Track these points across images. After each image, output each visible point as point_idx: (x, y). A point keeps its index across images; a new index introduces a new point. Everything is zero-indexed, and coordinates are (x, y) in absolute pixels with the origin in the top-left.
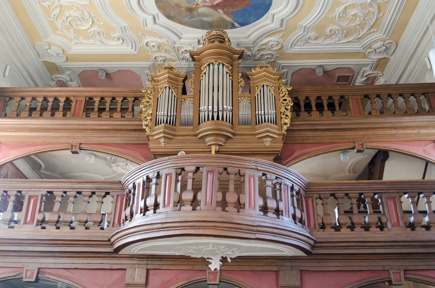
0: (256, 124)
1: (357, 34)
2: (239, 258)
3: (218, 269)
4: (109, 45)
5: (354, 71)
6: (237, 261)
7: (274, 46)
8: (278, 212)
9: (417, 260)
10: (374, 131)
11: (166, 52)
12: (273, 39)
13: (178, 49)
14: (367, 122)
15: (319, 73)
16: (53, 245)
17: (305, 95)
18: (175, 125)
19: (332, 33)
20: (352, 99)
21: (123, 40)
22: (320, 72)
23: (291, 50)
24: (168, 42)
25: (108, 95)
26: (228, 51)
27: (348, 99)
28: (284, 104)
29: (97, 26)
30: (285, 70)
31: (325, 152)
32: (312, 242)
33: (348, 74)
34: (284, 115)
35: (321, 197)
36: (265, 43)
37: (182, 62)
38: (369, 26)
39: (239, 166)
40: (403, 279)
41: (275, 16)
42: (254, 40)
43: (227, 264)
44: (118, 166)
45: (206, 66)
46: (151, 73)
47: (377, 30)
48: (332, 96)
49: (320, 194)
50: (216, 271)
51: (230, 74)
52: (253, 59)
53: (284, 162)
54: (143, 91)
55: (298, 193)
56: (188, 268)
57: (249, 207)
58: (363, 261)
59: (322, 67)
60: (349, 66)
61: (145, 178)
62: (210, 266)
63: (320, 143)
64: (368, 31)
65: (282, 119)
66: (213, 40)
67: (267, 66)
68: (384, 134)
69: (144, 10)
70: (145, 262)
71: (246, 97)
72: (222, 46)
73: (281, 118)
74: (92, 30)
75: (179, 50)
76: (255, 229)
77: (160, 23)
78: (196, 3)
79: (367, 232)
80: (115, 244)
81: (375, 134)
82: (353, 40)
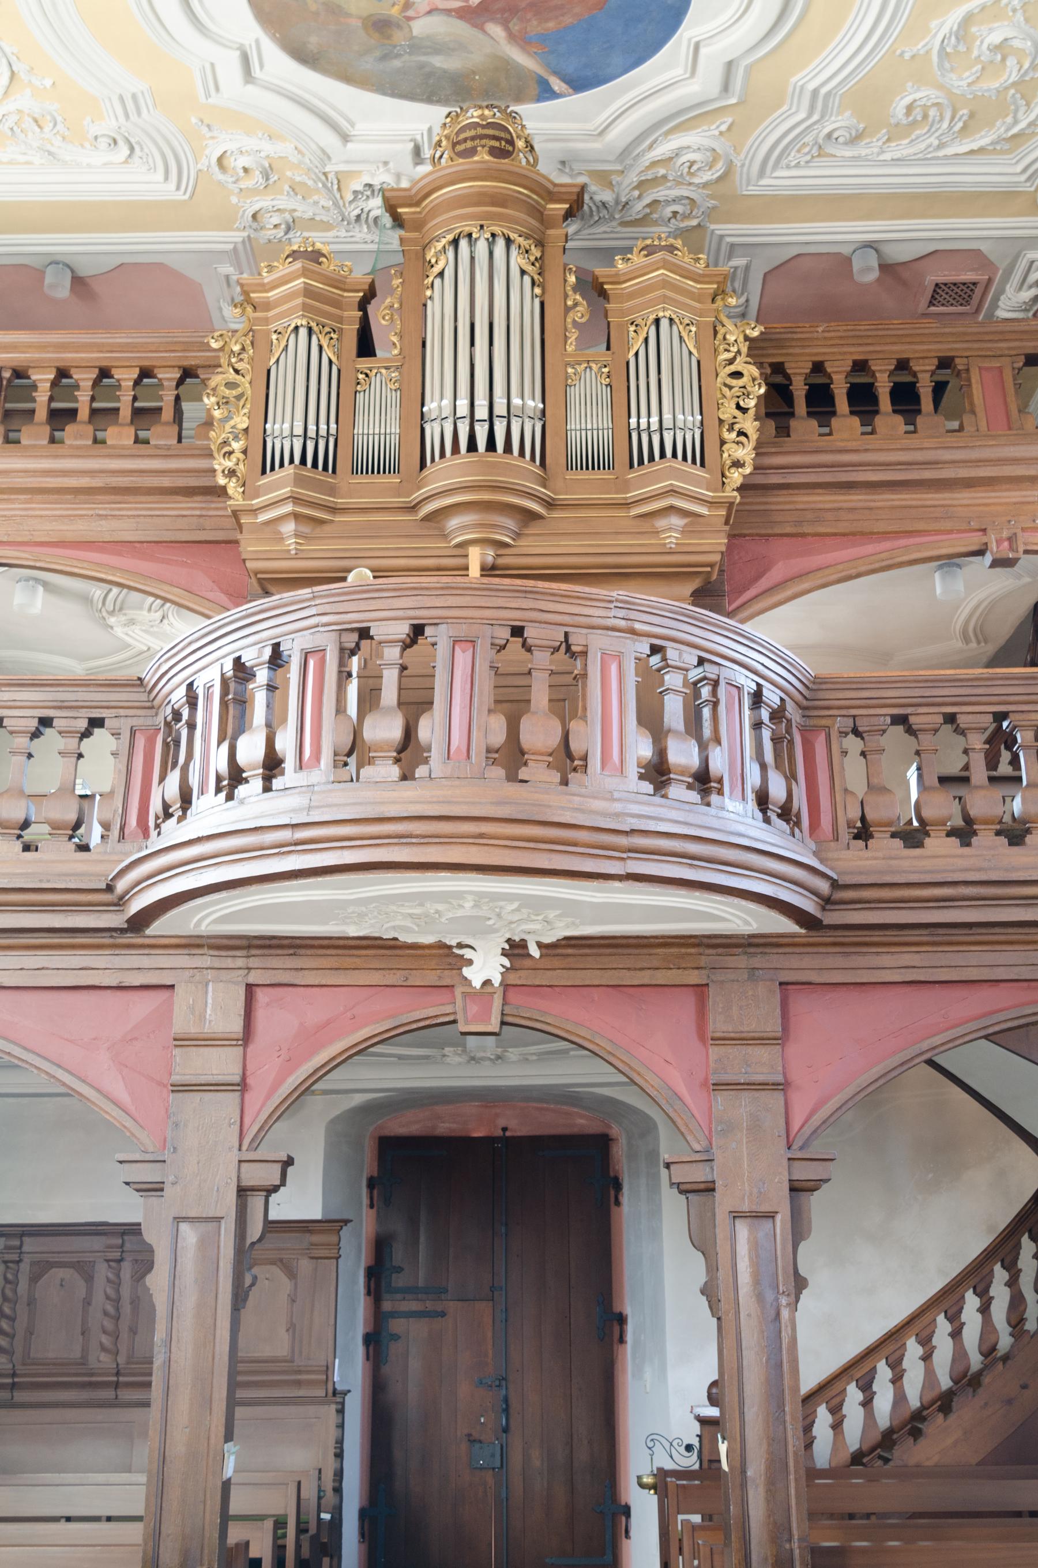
0: (631, 466)
1: (1009, 119)
2: (570, 942)
3: (497, 980)
5: (992, 263)
7: (699, 169)
11: (296, 194)
18: (334, 471)
21: (132, 149)
22: (869, 269)
23: (764, 182)
24: (300, 152)
25: (82, 359)
28: (733, 390)
31: (877, 565)
32: (824, 886)
33: (968, 277)
34: (731, 429)
35: (860, 729)
37: (357, 229)
41: (703, 51)
43: (527, 963)
44: (132, 622)
45: (444, 247)
46: (242, 273)
49: (854, 717)
50: (488, 989)
51: (536, 277)
54: (214, 345)
55: (777, 715)
57: (603, 768)
62: (466, 972)
63: (862, 534)
65: (726, 447)
66: (469, 144)
67: (672, 246)
69: (203, 25)
70: (240, 962)
71: (593, 366)
73: (723, 443)
76: (623, 841)
79: (1015, 849)
82: (992, 143)
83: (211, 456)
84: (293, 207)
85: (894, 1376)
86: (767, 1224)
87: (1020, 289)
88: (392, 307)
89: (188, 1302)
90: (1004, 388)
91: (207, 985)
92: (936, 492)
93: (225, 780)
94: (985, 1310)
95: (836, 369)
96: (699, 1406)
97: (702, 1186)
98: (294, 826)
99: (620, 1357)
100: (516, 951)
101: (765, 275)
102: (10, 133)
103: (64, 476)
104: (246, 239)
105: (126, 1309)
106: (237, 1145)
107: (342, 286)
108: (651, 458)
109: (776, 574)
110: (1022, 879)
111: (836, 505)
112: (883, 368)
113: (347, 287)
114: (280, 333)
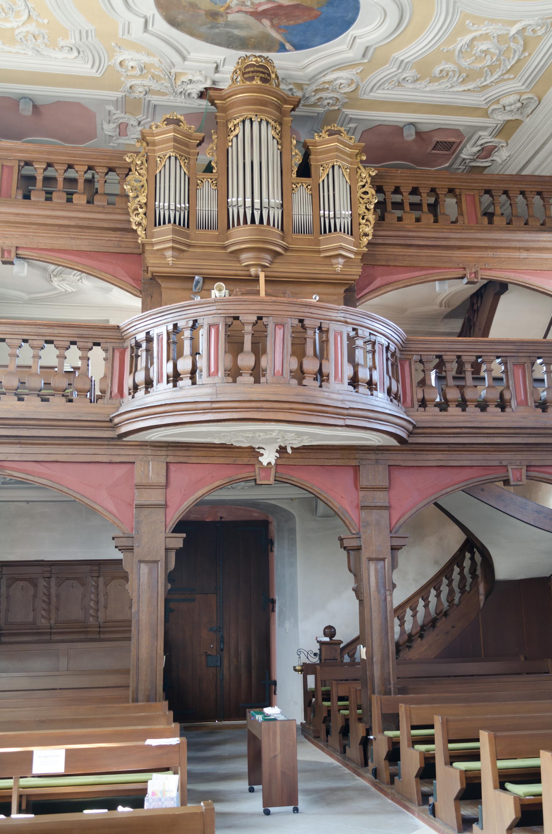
0: (321, 233)
1: (483, 79)
2: (305, 448)
3: (273, 463)
5: (463, 135)
6: (301, 452)
7: (344, 87)
8: (371, 385)
9: (545, 453)
10: (496, 252)
11: (154, 79)
12: (344, 75)
13: (176, 75)
14: (488, 237)
15: (409, 135)
16: (19, 427)
17: (394, 183)
18: (188, 227)
19: (444, 75)
20: (466, 195)
21: (79, 53)
22: (411, 135)
23: (372, 94)
24: (161, 62)
25: (59, 159)
26: (275, 97)
27: (460, 195)
28: (364, 200)
29: (34, 24)
30: (352, 125)
31: (420, 281)
32: (410, 427)
33: (452, 140)
34: (363, 219)
35: (423, 360)
36: (329, 81)
38: (503, 70)
39: (322, 317)
40: (524, 477)
41: (358, 41)
43: (286, 455)
44: (64, 280)
45: (238, 123)
46: (117, 110)
47: (515, 77)
48: (435, 188)
49: (421, 355)
50: (270, 466)
51: (279, 140)
52: (305, 103)
53: (357, 295)
54: (128, 160)
55: (393, 355)
56: (229, 461)
57: (335, 380)
58: (474, 453)
59: (414, 126)
61: (171, 327)
62: (260, 459)
63: (414, 267)
64: (499, 77)
65: (361, 226)
66: (251, 75)
67: (339, 131)
68: (510, 258)
69: (131, 7)
70: (164, 453)
71: (304, 184)
72: (267, 88)
73: (360, 224)
74: (24, 29)
76: (345, 412)
77: (155, 31)
78: (227, 5)
79: (483, 413)
80: (120, 426)
81: (497, 256)
82: (474, 88)
83: (128, 214)
84: (151, 85)
85: (400, 624)
86: (382, 563)
87: (473, 146)
88: (212, 149)
89: (145, 597)
90: (475, 204)
91: (149, 463)
92: (446, 251)
93: (171, 377)
94: (438, 596)
95: (404, 190)
96: (319, 637)
97: (356, 548)
98: (212, 402)
99: (272, 618)
100: (282, 451)
101: (363, 132)
102: (20, 41)
103: (57, 219)
104: (124, 96)
105: (54, 599)
106: (164, 530)
107: (190, 137)
108: (330, 231)
109: (377, 283)
110: (487, 426)
111: (404, 253)
112: (425, 191)
113: (192, 138)
114: (161, 158)
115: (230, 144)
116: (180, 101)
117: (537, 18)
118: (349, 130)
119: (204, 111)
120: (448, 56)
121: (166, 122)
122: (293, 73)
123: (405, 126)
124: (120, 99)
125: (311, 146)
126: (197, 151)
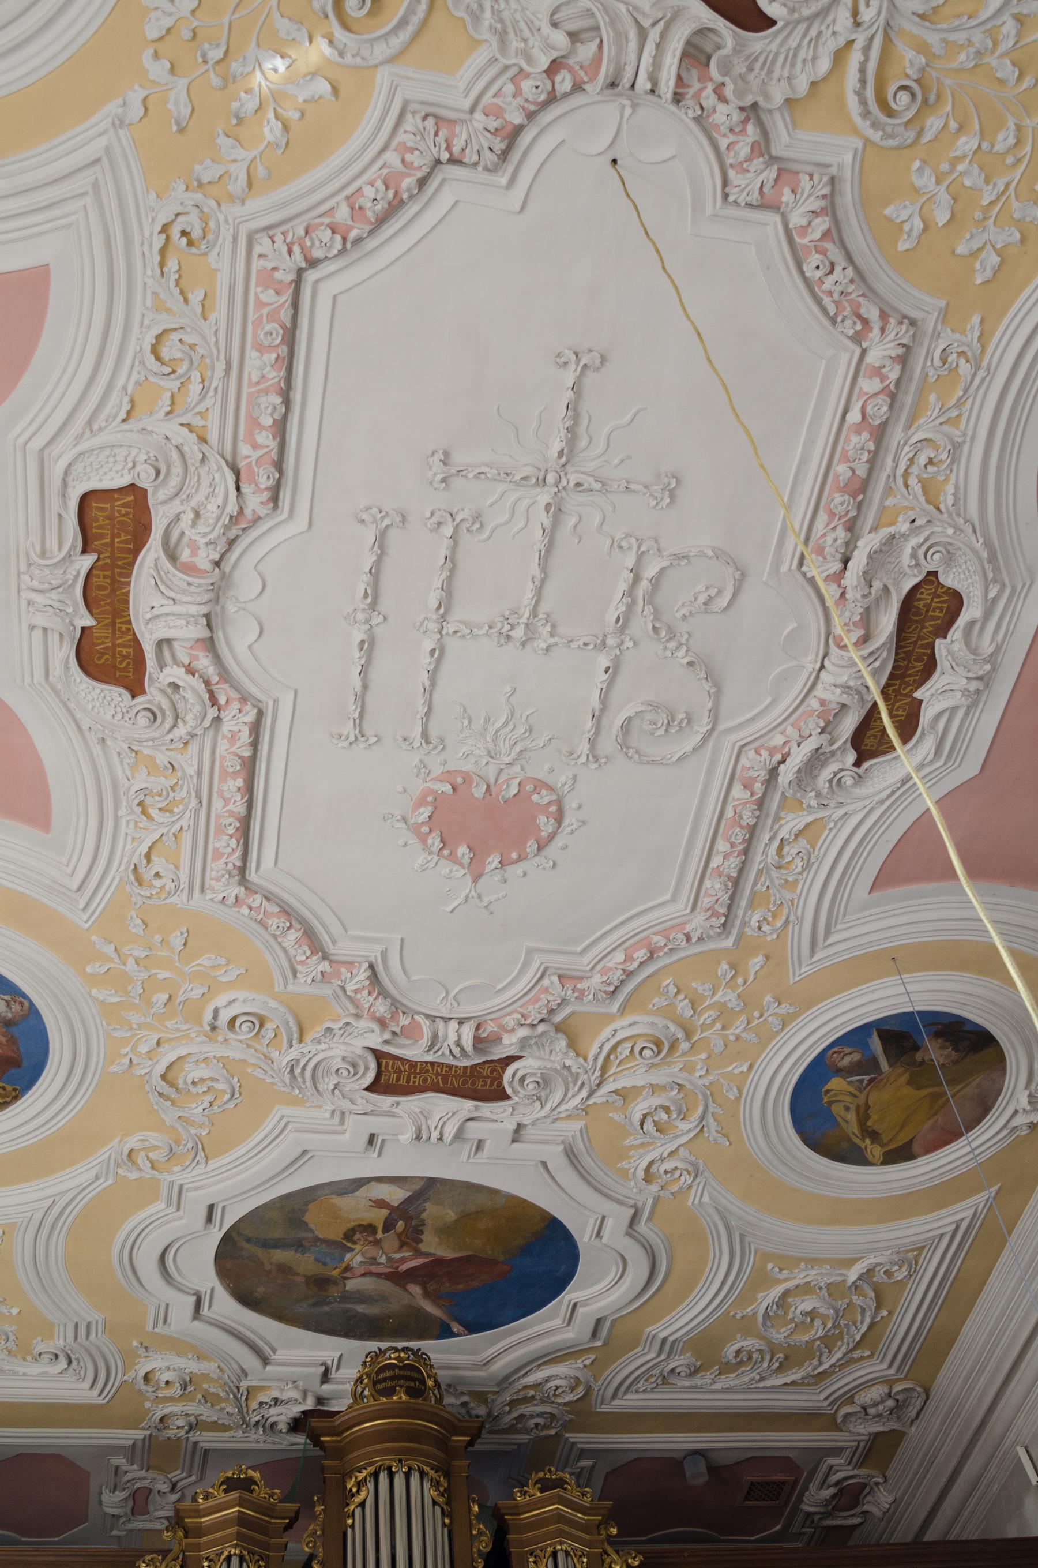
1: (815, 1362)
4: (15, 1373)
11: (206, 1402)
15: (697, 1475)
19: (744, 1359)
21: (70, 1362)
23: (616, 1402)
24: (221, 1370)
30: (586, 1463)
33: (779, 1477)
37: (253, 1431)
38: (848, 1344)
41: (581, 1310)
42: (505, 1373)
45: (365, 1479)
51: (445, 1507)
59: (703, 1456)
60: (783, 1454)
64: (844, 1355)
66: (388, 1384)
67: (561, 1479)
75: (250, 1397)
78: (344, 1265)
87: (821, 1487)
88: (314, 1533)
101: (607, 1474)
115: (350, 1521)
116: (256, 1439)
117: (889, 1252)
118: (580, 1473)
119: (300, 1455)
120: (746, 1325)
121: (225, 1487)
122: (467, 1373)
123: (685, 1457)
124: (140, 1443)
125: (509, 1514)
126: (285, 1540)
